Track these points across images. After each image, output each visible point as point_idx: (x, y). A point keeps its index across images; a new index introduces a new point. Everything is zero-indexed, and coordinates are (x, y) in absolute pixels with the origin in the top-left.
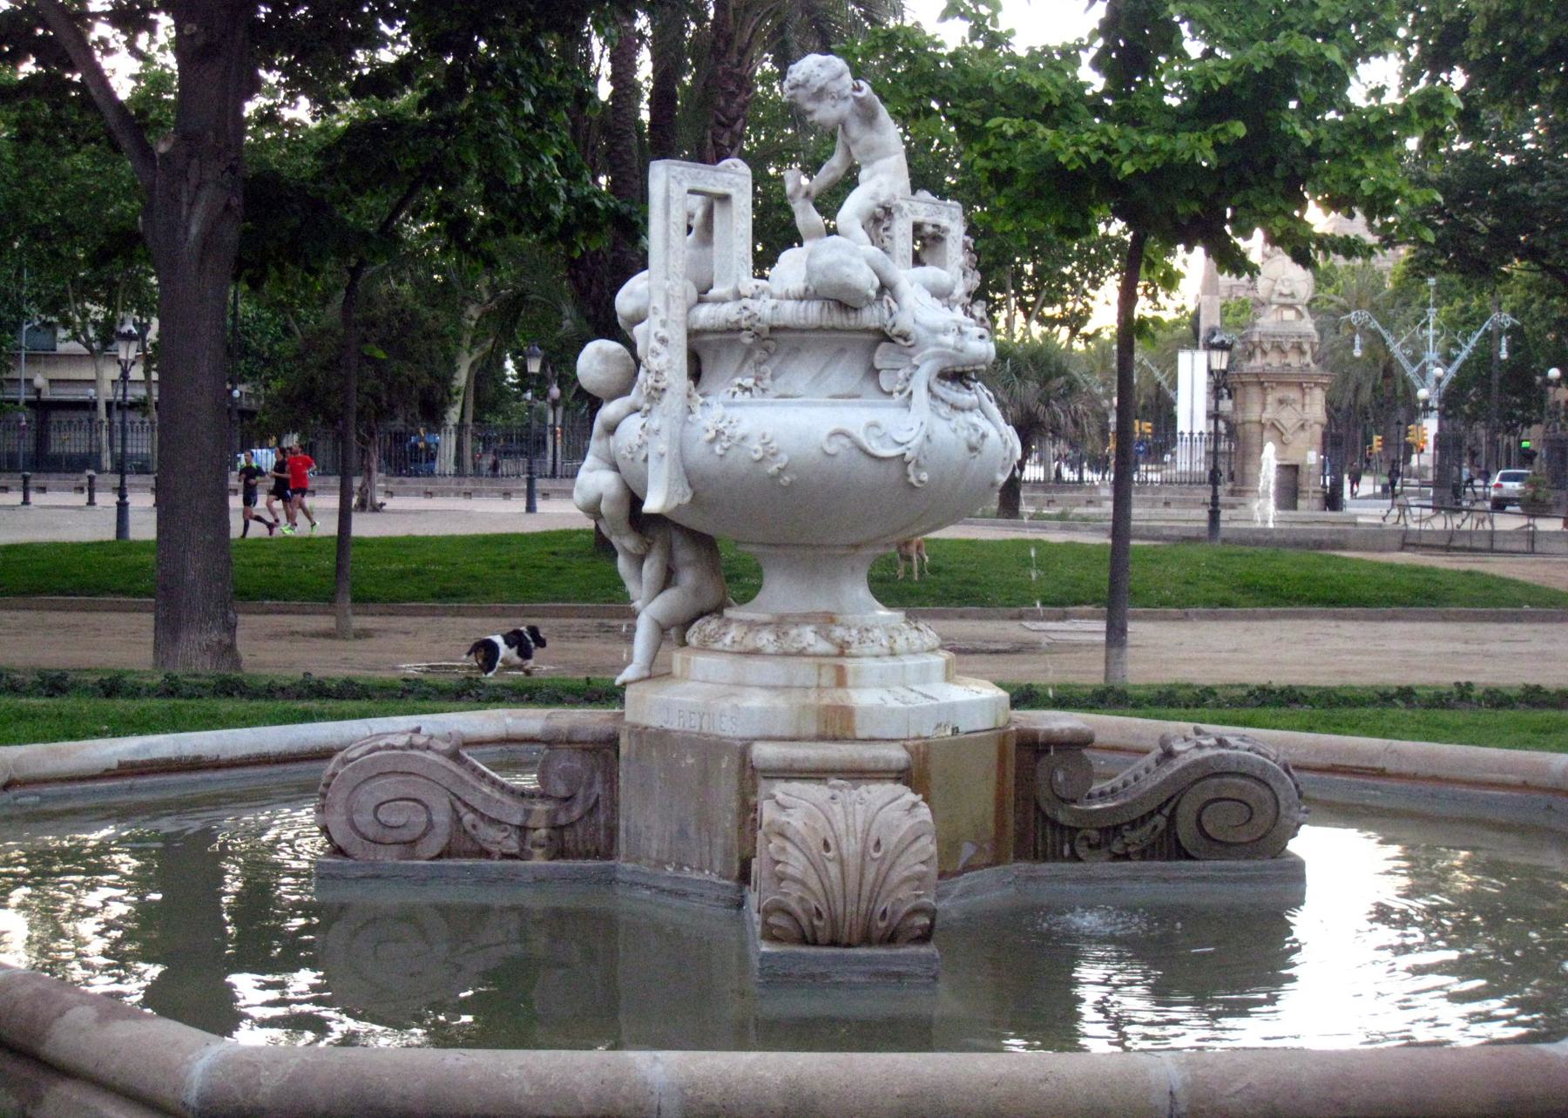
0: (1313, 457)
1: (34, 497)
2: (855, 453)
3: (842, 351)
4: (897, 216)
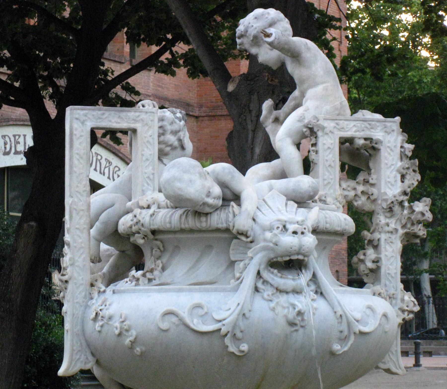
1: (425, 361)
2: (182, 327)
3: (209, 247)
4: (320, 134)
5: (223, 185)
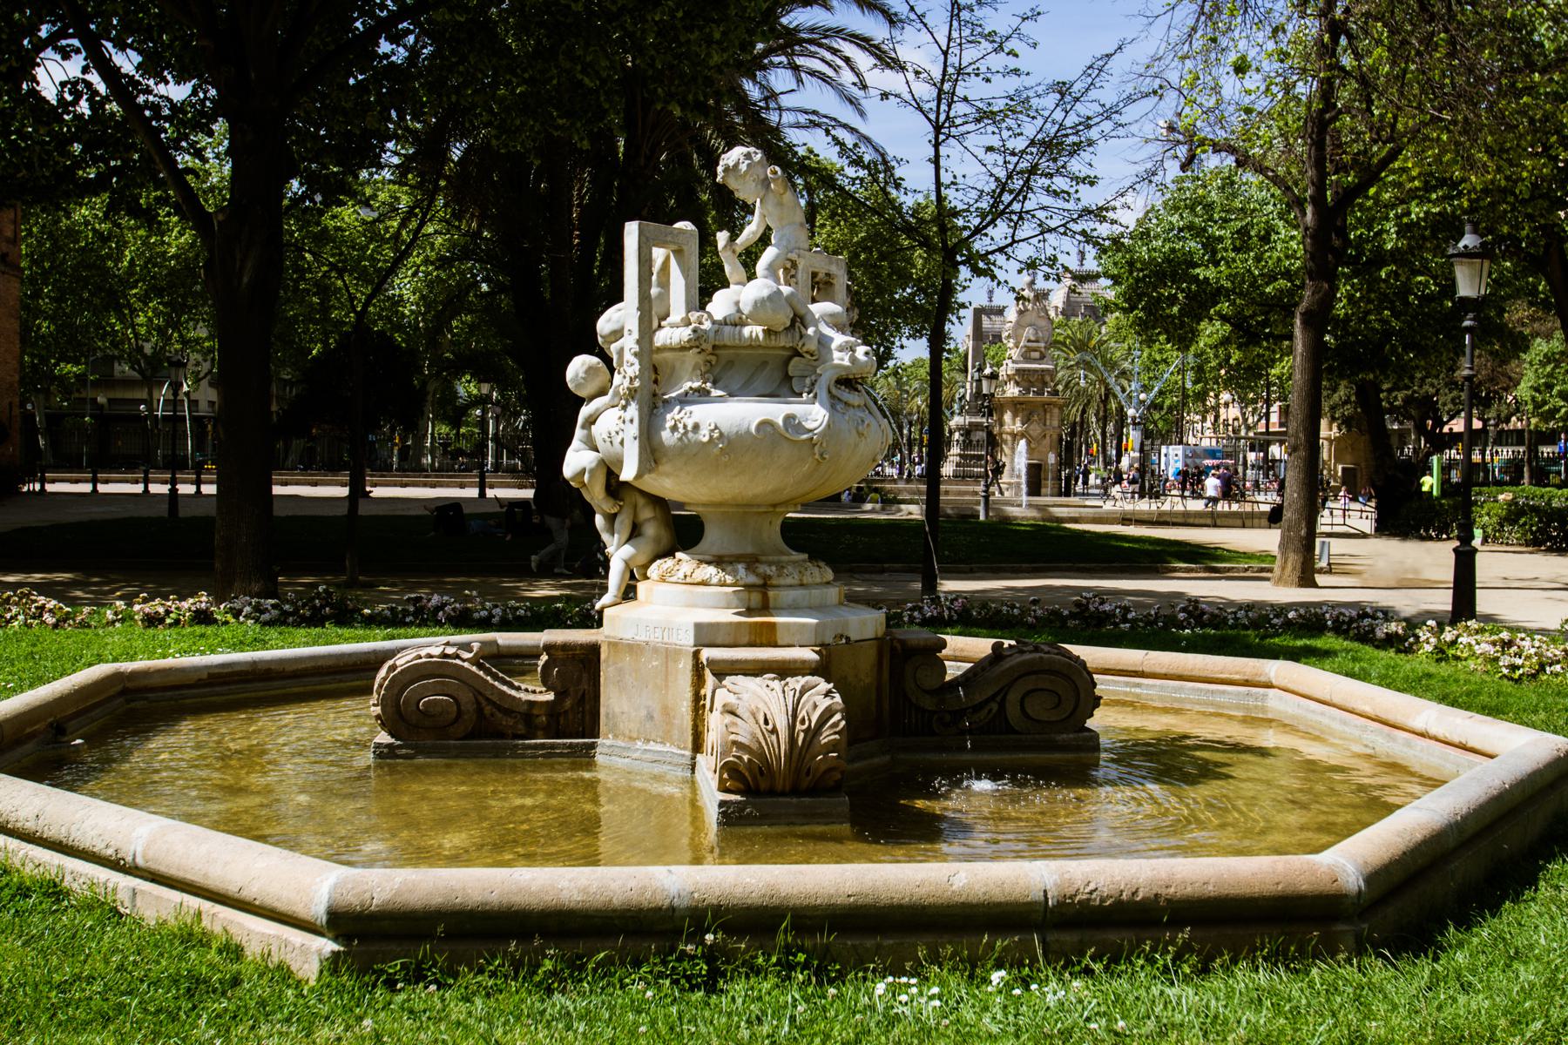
0: (1052, 459)
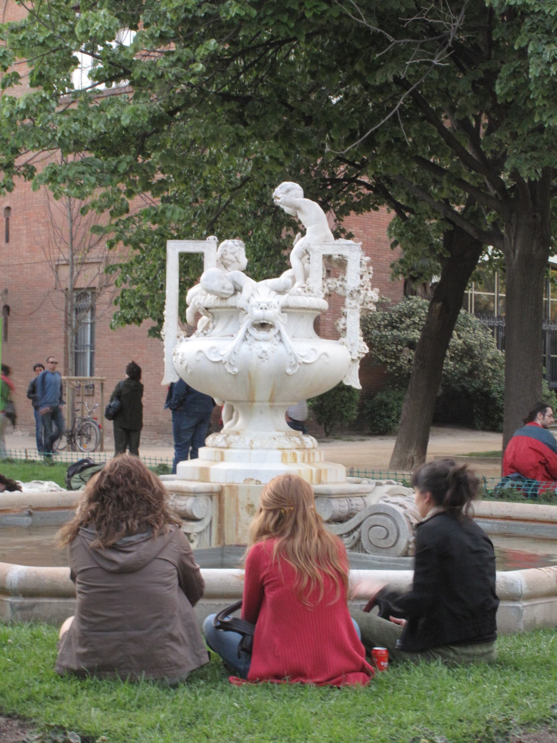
4: (310, 253)
5: (234, 283)
